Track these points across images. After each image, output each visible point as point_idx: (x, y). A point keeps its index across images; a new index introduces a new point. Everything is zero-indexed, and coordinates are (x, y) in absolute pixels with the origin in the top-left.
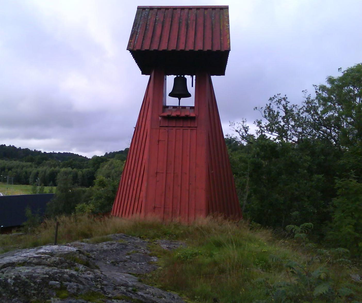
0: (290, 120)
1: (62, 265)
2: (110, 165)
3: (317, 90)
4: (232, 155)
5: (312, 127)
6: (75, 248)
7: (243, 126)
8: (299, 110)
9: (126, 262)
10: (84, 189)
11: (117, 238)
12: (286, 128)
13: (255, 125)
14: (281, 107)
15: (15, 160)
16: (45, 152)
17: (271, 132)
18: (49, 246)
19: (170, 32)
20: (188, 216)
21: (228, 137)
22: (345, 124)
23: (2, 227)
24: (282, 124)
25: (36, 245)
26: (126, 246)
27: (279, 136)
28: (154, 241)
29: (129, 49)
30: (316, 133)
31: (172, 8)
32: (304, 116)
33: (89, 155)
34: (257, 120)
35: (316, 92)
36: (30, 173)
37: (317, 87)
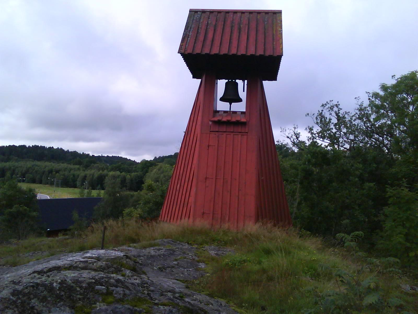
0: (342, 127)
1: (109, 270)
2: (159, 170)
3: (370, 97)
4: (282, 161)
5: (364, 135)
6: (123, 253)
7: (294, 132)
10: (132, 193)
11: (165, 244)
12: (338, 135)
13: (307, 131)
14: (334, 114)
15: (63, 163)
16: (93, 155)
17: (323, 139)
19: (222, 36)
21: (279, 143)
24: (334, 131)
25: (82, 249)
26: (174, 251)
27: (331, 143)
30: (369, 140)
31: (225, 12)
33: (138, 159)
35: (369, 99)
36: (78, 176)
37: (370, 94)
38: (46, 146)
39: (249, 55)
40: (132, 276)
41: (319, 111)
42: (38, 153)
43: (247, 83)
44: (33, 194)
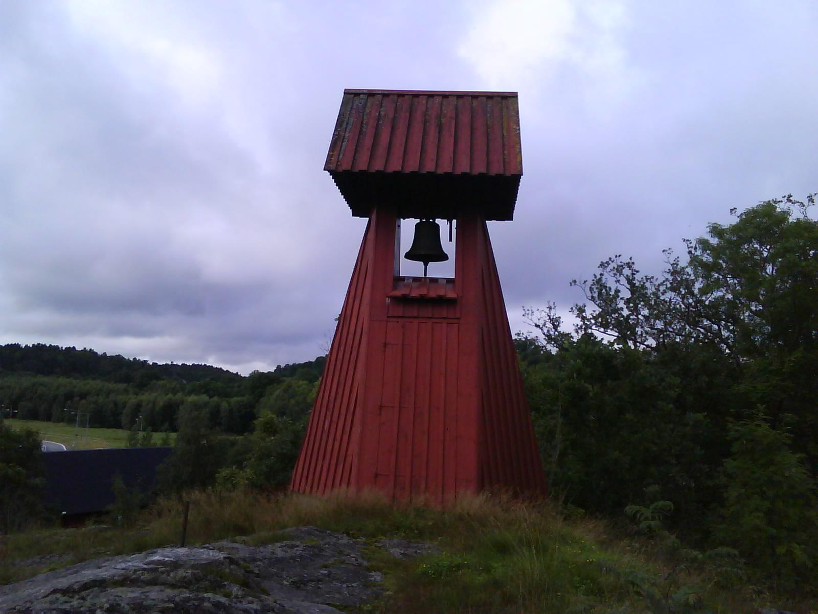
0: (639, 306)
1: (198, 585)
3: (690, 249)
4: (528, 373)
5: (683, 319)
6: (222, 554)
7: (549, 316)
8: (657, 287)
9: (320, 583)
10: (232, 438)
11: (303, 535)
12: (633, 321)
13: (573, 314)
14: (623, 281)
15: (94, 379)
16: (155, 362)
17: (604, 329)
18: (171, 549)
20: (443, 493)
21: (520, 338)
22: (747, 314)
23: (65, 514)
24: (626, 312)
25: (140, 548)
26: (322, 550)
27: (620, 336)
28: (376, 542)
29: (329, 169)
30: (692, 330)
32: (668, 298)
33: (245, 371)
34: (577, 305)
35: (690, 252)
37: (691, 243)
38: (60, 346)
39: (459, 173)
40: (244, 597)
41: (594, 275)
42: (43, 358)
43: (457, 226)
44: (35, 440)
